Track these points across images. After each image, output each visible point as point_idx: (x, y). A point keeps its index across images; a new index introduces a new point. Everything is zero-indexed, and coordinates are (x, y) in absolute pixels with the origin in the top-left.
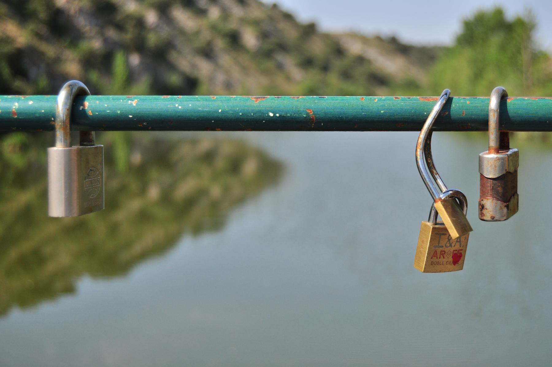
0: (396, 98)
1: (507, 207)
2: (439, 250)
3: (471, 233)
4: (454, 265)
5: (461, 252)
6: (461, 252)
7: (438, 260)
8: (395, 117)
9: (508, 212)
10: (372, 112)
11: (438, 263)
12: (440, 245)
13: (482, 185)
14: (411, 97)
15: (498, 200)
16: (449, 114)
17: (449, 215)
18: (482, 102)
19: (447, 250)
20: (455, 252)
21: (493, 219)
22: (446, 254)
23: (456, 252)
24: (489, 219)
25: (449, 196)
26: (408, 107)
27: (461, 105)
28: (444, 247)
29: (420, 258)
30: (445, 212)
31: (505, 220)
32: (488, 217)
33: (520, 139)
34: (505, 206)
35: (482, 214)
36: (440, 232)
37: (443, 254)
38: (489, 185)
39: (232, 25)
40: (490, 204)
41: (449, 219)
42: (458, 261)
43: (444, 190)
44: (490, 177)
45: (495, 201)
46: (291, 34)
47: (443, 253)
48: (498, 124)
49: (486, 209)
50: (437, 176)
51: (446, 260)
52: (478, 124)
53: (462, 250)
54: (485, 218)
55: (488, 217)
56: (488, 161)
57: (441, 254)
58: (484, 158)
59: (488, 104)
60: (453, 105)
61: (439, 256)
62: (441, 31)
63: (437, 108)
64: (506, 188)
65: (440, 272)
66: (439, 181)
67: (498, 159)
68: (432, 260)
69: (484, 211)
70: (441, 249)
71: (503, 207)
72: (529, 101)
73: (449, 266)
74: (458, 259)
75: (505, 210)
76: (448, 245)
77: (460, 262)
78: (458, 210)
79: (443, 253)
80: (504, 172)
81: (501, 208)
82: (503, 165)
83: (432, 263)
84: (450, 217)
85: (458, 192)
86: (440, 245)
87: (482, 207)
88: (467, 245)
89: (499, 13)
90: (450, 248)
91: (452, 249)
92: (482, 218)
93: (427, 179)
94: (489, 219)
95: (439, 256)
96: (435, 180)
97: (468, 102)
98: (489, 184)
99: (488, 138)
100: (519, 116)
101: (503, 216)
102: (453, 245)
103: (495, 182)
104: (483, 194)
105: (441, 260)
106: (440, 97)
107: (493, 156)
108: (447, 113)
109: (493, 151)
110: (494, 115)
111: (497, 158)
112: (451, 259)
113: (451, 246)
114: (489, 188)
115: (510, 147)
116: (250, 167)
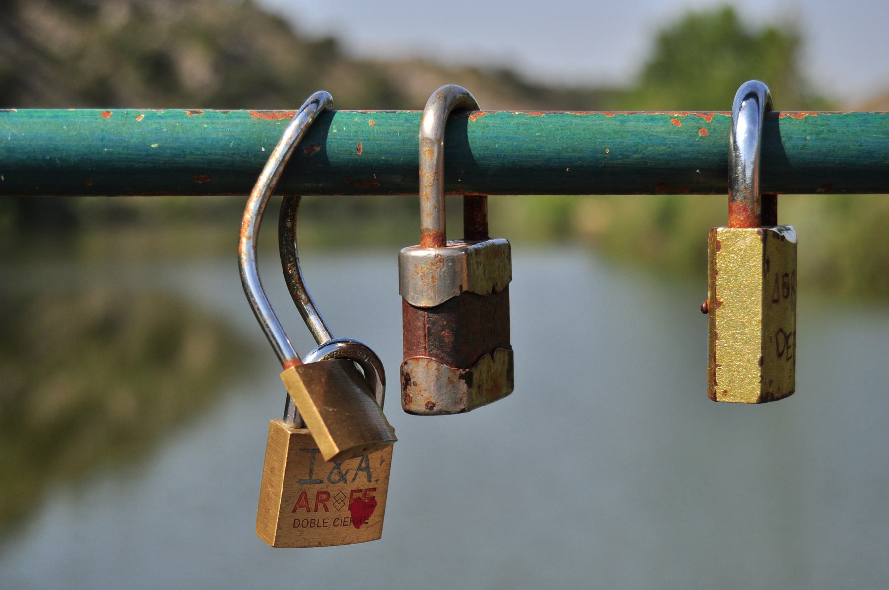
0: (192, 113)
1: (468, 379)
2: (312, 491)
3: (395, 444)
4: (357, 526)
5: (374, 494)
6: (374, 494)
7: (312, 515)
8: (188, 158)
9: (470, 394)
10: (127, 147)
11: (312, 524)
12: (314, 477)
13: (408, 327)
14: (231, 111)
15: (441, 361)
16: (324, 150)
17: (315, 402)
18: (407, 120)
19: (333, 490)
20: (356, 495)
21: (431, 410)
22: (332, 500)
23: (360, 495)
24: (423, 408)
25: (332, 355)
26: (221, 135)
27: (353, 129)
28: (326, 482)
29: (267, 511)
30: (306, 392)
31: (463, 411)
32: (419, 404)
33: (515, 214)
34: (461, 377)
35: (406, 398)
36: (303, 445)
37: (323, 502)
38: (420, 324)
39: (155, 38)
40: (427, 372)
41: (315, 409)
42: (367, 517)
43: (324, 339)
44: (422, 304)
45: (434, 365)
46: (283, 59)
47: (323, 498)
48: (441, 173)
49: (416, 385)
50: (307, 308)
51: (332, 514)
52: (392, 177)
53: (375, 489)
54: (413, 407)
55: (419, 404)
56: (416, 266)
57: (318, 500)
58: (408, 257)
59: (419, 125)
60: (334, 129)
61: (312, 505)
62: (615, 55)
63: (290, 133)
64: (473, 336)
65: (332, 545)
66: (313, 319)
67: (439, 260)
68: (296, 516)
69: (411, 390)
70: (317, 487)
71: (456, 379)
72: (524, 121)
73: (341, 529)
74: (364, 510)
75: (463, 386)
76: (335, 477)
77: (372, 520)
78: (358, 390)
79: (323, 498)
80: (457, 293)
81: (450, 381)
82: (454, 274)
83: (296, 524)
84: (317, 406)
85: (360, 345)
86: (314, 477)
87: (406, 380)
88: (387, 477)
89: (728, 17)
90: (342, 484)
91: (348, 489)
92: (407, 408)
93: (264, 312)
94: (423, 408)
95: (312, 505)
96: (305, 316)
97: (370, 122)
98: (421, 321)
99: (416, 209)
100: (498, 157)
101: (456, 403)
102: (350, 477)
103: (433, 317)
104: (409, 348)
105: (320, 515)
106: (297, 111)
107: (431, 252)
108: (317, 149)
109: (429, 240)
110: (431, 152)
111: (436, 256)
112: (346, 513)
113: (343, 479)
114: (421, 333)
115: (490, 235)
116: (197, 353)
